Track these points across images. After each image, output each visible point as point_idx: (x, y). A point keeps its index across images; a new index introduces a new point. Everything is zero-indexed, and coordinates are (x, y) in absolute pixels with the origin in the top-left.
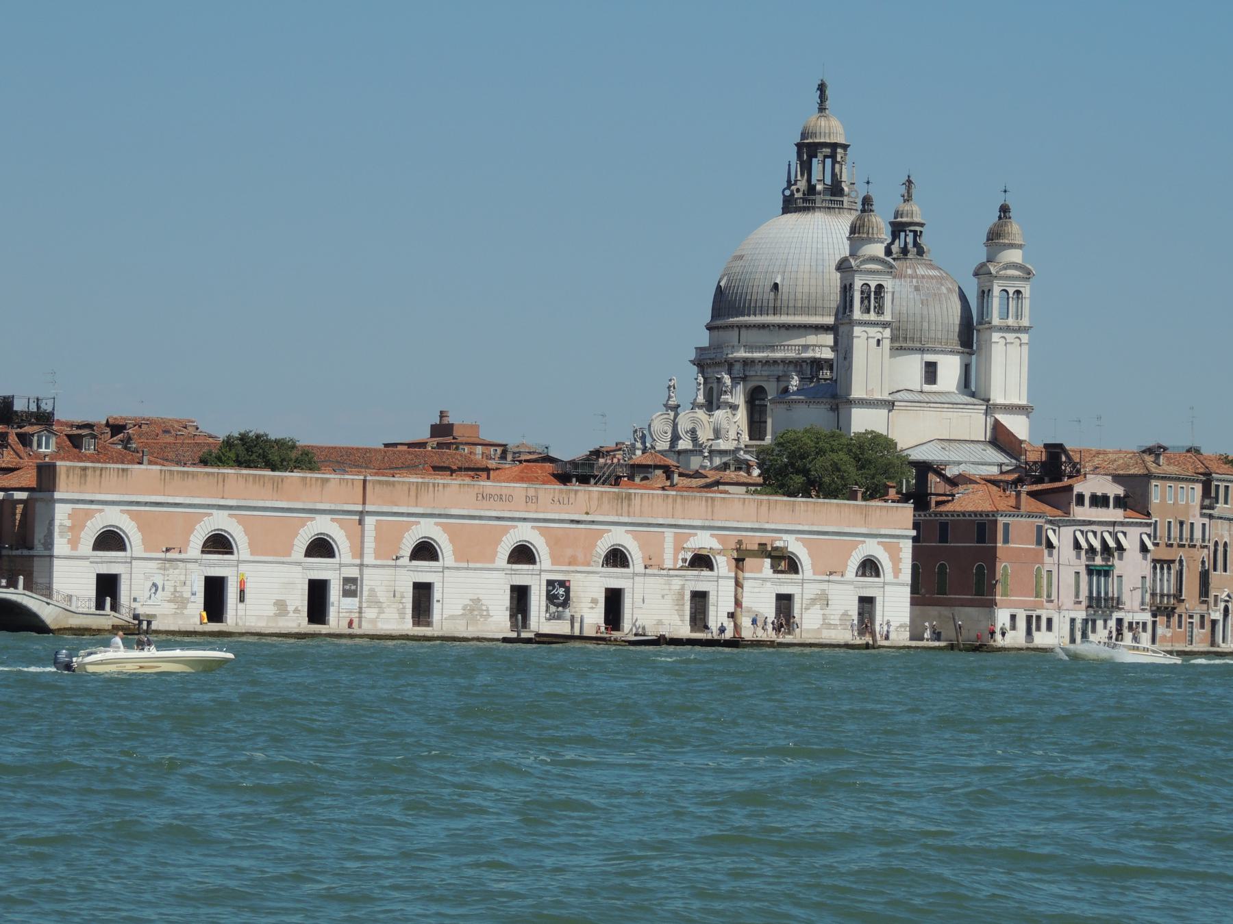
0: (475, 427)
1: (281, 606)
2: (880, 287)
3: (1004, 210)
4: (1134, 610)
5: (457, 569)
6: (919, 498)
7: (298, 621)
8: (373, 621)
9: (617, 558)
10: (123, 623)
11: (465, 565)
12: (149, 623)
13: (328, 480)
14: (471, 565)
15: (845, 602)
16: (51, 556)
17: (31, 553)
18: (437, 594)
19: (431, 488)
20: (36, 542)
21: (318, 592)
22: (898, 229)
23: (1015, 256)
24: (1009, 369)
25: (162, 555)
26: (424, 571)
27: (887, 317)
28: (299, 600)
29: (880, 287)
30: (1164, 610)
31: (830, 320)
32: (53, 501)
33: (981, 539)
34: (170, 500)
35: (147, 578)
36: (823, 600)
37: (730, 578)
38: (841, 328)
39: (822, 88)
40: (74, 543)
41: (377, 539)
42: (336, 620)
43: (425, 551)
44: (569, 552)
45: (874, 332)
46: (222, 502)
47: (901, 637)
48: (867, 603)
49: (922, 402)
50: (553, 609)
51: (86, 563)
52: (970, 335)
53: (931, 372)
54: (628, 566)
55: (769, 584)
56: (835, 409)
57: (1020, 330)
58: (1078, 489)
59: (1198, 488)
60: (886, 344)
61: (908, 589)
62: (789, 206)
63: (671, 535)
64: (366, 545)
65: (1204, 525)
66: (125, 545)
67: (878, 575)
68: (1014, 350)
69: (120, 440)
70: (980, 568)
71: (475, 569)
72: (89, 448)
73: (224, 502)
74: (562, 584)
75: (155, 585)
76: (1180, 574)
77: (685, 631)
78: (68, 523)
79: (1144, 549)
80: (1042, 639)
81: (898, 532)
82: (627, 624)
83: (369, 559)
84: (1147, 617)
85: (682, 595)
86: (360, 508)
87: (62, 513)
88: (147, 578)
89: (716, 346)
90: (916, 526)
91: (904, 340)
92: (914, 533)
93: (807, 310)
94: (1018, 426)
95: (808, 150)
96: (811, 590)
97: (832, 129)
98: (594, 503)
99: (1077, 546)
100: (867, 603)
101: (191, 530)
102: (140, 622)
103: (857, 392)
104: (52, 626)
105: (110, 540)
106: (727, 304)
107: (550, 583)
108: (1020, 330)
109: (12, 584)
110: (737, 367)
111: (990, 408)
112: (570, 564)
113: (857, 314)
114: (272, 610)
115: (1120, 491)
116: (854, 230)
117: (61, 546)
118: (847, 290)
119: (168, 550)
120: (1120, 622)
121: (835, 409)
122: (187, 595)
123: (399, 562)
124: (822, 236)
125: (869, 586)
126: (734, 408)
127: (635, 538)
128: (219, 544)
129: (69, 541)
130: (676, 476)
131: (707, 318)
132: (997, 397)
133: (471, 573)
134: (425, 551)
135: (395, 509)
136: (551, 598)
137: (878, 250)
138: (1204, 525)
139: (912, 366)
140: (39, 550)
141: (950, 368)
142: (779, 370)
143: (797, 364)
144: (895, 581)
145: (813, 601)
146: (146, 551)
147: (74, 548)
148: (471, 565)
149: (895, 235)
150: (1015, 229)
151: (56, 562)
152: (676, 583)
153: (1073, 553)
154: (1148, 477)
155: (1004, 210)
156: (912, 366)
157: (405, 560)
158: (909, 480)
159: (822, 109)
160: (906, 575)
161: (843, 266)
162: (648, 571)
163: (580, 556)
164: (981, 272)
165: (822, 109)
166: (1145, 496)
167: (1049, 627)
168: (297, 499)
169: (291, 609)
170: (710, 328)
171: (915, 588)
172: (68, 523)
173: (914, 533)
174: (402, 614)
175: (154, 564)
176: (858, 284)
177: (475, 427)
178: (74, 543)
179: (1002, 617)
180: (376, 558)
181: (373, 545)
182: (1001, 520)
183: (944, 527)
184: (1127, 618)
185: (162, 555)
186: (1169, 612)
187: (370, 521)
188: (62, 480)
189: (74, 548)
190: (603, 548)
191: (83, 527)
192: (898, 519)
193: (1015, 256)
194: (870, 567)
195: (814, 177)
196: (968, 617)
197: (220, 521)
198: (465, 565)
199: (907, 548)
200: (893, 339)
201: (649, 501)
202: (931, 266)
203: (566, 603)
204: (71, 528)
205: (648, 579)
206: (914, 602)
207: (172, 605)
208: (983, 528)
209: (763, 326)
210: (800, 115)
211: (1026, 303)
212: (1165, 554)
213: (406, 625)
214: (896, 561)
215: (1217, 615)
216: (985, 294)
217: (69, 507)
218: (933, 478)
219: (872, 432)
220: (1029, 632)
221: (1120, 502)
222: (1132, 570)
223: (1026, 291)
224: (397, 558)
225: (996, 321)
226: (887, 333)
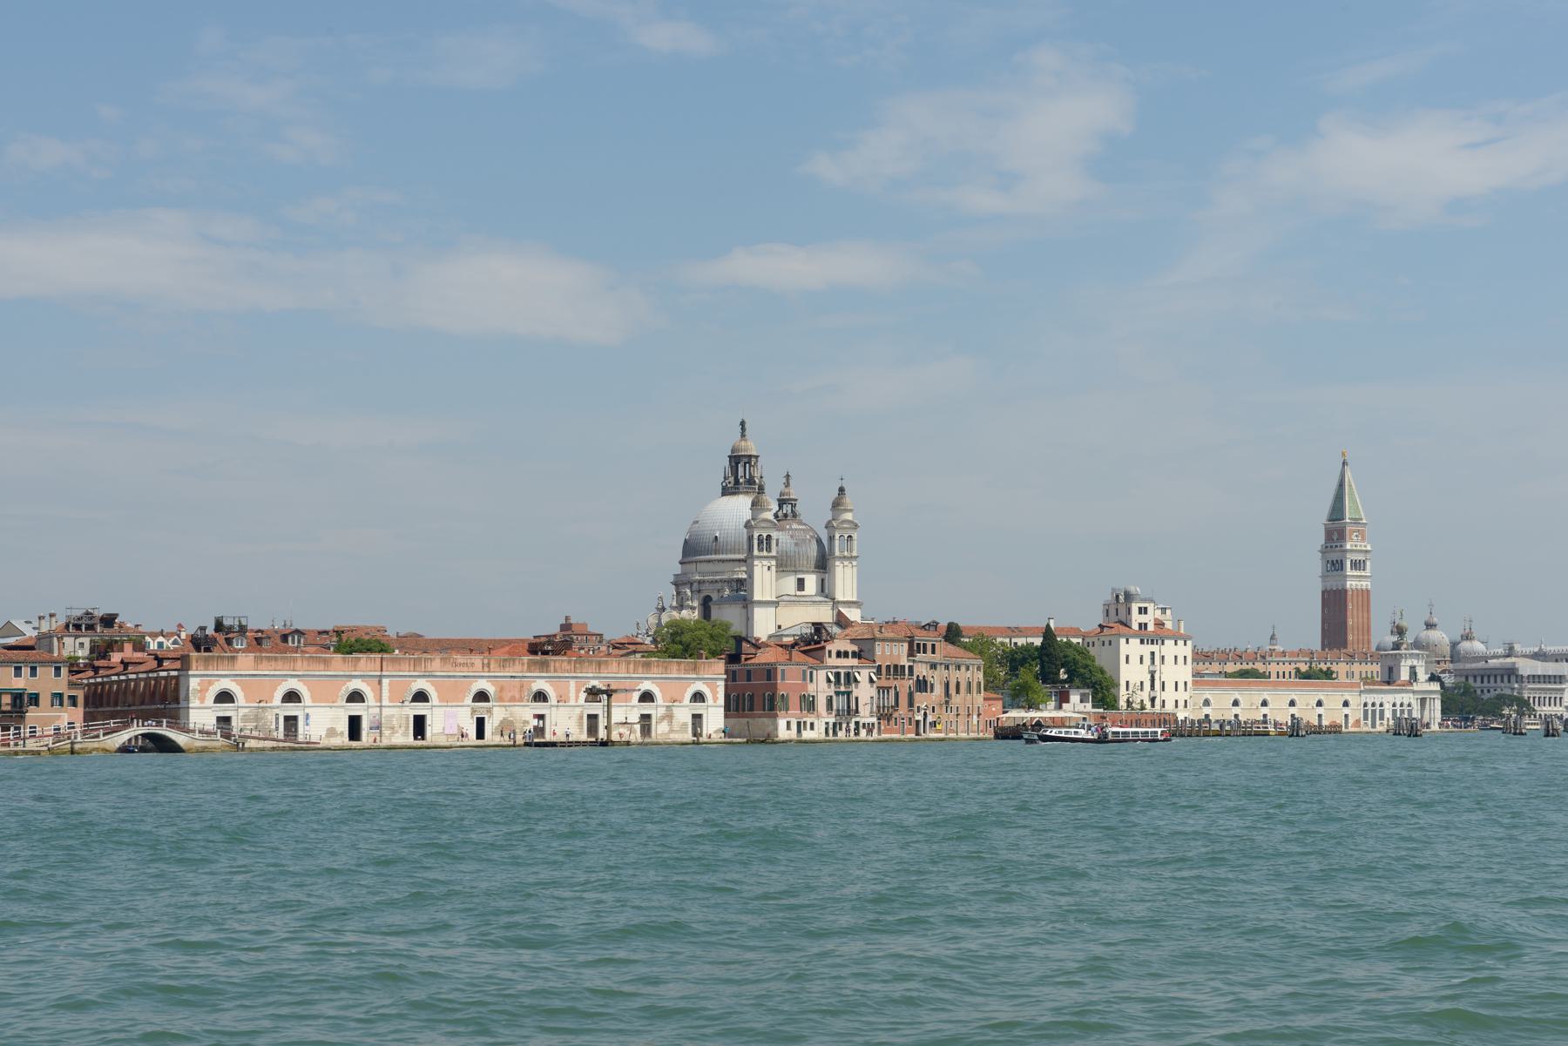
0: (585, 625)
2: (769, 537)
3: (842, 490)
4: (866, 716)
6: (733, 658)
7: (343, 740)
15: (683, 715)
18: (428, 722)
22: (781, 503)
23: (848, 516)
24: (845, 581)
26: (420, 709)
27: (774, 553)
28: (344, 727)
29: (769, 537)
30: (885, 715)
31: (742, 556)
33: (769, 679)
38: (747, 561)
39: (743, 424)
40: (202, 700)
42: (367, 737)
45: (765, 562)
47: (717, 737)
48: (697, 718)
49: (794, 602)
52: (823, 564)
53: (801, 584)
56: (746, 607)
57: (852, 558)
58: (828, 648)
59: (906, 645)
62: (726, 492)
65: (1153, 654)
68: (848, 570)
69: (212, 641)
72: (266, 645)
73: (359, 673)
76: (897, 695)
77: (584, 737)
79: (871, 681)
80: (807, 735)
83: (385, 702)
84: (874, 720)
87: (194, 683)
89: (684, 574)
90: (726, 672)
91: (785, 565)
93: (733, 551)
94: (853, 615)
95: (736, 460)
96: (662, 711)
97: (750, 447)
99: (829, 680)
100: (697, 718)
101: (275, 689)
103: (756, 598)
106: (691, 550)
108: (852, 558)
109: (159, 724)
110: (695, 586)
111: (835, 603)
113: (756, 552)
115: (856, 648)
116: (753, 504)
118: (750, 538)
120: (857, 723)
121: (746, 607)
124: (741, 505)
125: (698, 708)
126: (693, 608)
131: (680, 557)
132: (839, 597)
134: (421, 697)
137: (769, 515)
138: (1153, 654)
139: (790, 583)
140: (183, 704)
141: (811, 581)
142: (719, 586)
143: (729, 581)
145: (663, 718)
149: (780, 507)
150: (848, 500)
153: (825, 685)
154: (874, 639)
155: (842, 490)
156: (790, 583)
157: (469, 700)
158: (730, 647)
159: (743, 435)
160: (721, 701)
161: (748, 525)
164: (828, 526)
165: (743, 435)
166: (872, 651)
167: (812, 727)
171: (727, 707)
174: (405, 734)
176: (756, 535)
177: (585, 625)
179: (782, 723)
182: (780, 668)
183: (749, 672)
184: (862, 721)
186: (889, 718)
187: (385, 682)
188: (194, 665)
192: (718, 667)
193: (848, 516)
194: (698, 697)
195: (740, 474)
196: (759, 724)
197: (293, 684)
199: (721, 684)
202: (801, 523)
206: (726, 716)
208: (770, 673)
209: (723, 561)
210: (729, 440)
211: (855, 543)
212: (884, 683)
213: (410, 740)
215: (919, 717)
216: (831, 539)
217: (198, 680)
220: (799, 731)
221: (854, 655)
222: (865, 692)
223: (855, 536)
225: (837, 553)
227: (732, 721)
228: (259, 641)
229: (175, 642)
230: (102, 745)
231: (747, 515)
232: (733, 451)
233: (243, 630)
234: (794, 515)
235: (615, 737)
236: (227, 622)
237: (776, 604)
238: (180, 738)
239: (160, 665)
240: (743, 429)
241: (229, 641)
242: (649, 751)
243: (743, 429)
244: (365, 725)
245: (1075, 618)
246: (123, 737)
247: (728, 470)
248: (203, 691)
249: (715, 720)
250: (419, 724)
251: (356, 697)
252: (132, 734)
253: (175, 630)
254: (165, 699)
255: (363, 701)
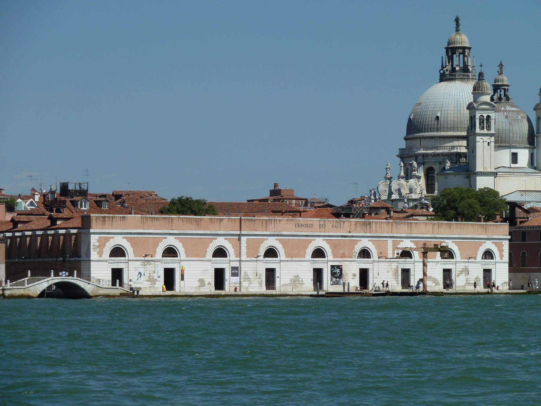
1: (202, 281)
2: (488, 117)
5: (287, 261)
6: (511, 220)
8: (247, 288)
9: (365, 253)
10: (125, 292)
11: (291, 259)
12: (138, 292)
13: (222, 219)
14: (294, 259)
15: (476, 271)
16: (90, 261)
17: (80, 259)
19: (273, 222)
20: (82, 254)
21: (219, 274)
22: (496, 88)
25: (143, 259)
26: (271, 263)
27: (493, 131)
28: (210, 278)
29: (488, 117)
31: (464, 134)
32: (90, 234)
34: (146, 231)
35: (136, 270)
36: (466, 271)
37: (237, 261)
38: (470, 138)
39: (457, 20)
40: (100, 254)
41: (247, 248)
43: (271, 253)
44: (341, 251)
45: (486, 138)
46: (172, 232)
47: (505, 288)
48: (487, 272)
49: (511, 172)
50: (334, 279)
51: (107, 263)
53: (514, 158)
54: (324, 257)
55: (439, 264)
56: (468, 177)
60: (492, 144)
61: (507, 265)
62: (443, 78)
63: (391, 241)
64: (242, 251)
66: (177, 254)
67: (492, 258)
69: (120, 203)
70: (524, 253)
71: (296, 261)
72: (105, 207)
73: (172, 232)
74: (339, 267)
75: (140, 273)
78: (97, 244)
81: (502, 237)
82: (371, 286)
83: (244, 257)
85: (397, 271)
86: (238, 233)
87: (94, 239)
88: (136, 270)
89: (409, 148)
90: (510, 234)
91: (501, 143)
92: (509, 237)
93: (453, 129)
95: (452, 50)
97: (463, 40)
98: (353, 227)
100: (487, 272)
101: (157, 246)
102: (134, 291)
103: (479, 169)
104: (91, 295)
105: (118, 252)
106: (414, 127)
107: (332, 267)
109: (71, 274)
110: (420, 158)
112: (342, 257)
113: (478, 130)
114: (197, 284)
116: (475, 89)
117: (94, 255)
118: (472, 118)
119: (146, 256)
121: (468, 177)
122: (156, 277)
123: (258, 259)
124: (460, 92)
125: (488, 264)
127: (374, 244)
128: (170, 252)
129: (98, 253)
130: (392, 212)
131: (405, 134)
133: (293, 263)
134: (271, 253)
135: (256, 233)
136: (333, 274)
137: (487, 98)
139: (505, 156)
140: (83, 257)
141: (524, 155)
143: (449, 156)
144: (501, 261)
145: (461, 272)
146: (135, 256)
147: (101, 256)
148: (294, 259)
149: (495, 91)
151: (92, 263)
152: (394, 265)
157: (261, 258)
160: (506, 258)
161: (470, 107)
162: (380, 260)
163: (347, 253)
168: (208, 229)
169: (206, 283)
170: (406, 139)
172: (97, 244)
173: (509, 237)
174: (261, 284)
175: (139, 263)
176: (478, 115)
177: (292, 191)
178: (100, 254)
180: (286, 257)
181: (388, 247)
183: (524, 233)
185: (143, 259)
187: (243, 239)
189: (101, 256)
190: (358, 248)
191: (104, 246)
195: (454, 64)
197: (171, 241)
198: (291, 259)
199: (506, 244)
200: (496, 142)
201: (381, 226)
203: (340, 276)
204: (98, 247)
205: (380, 264)
207: (149, 283)
213: (263, 290)
214: (501, 251)
218: (518, 210)
219: (487, 188)
224: (258, 257)
226: (493, 139)
227: (520, 275)
228: (99, 204)
229: (32, 204)
230: (26, 292)
231: (470, 99)
232: (449, 43)
233: (83, 193)
234: (508, 99)
235: (429, 289)
236: (71, 187)
237: (495, 174)
238: (88, 288)
239: (15, 226)
240: (458, 25)
241: (74, 204)
242: (447, 299)
243: (458, 25)
244: (227, 274)
245: (369, 190)
246: (43, 284)
247: (445, 58)
248: (101, 246)
249: (501, 276)
250: (270, 274)
251: (220, 253)
252: (50, 283)
253: (29, 193)
254: (71, 254)
255: (226, 256)
